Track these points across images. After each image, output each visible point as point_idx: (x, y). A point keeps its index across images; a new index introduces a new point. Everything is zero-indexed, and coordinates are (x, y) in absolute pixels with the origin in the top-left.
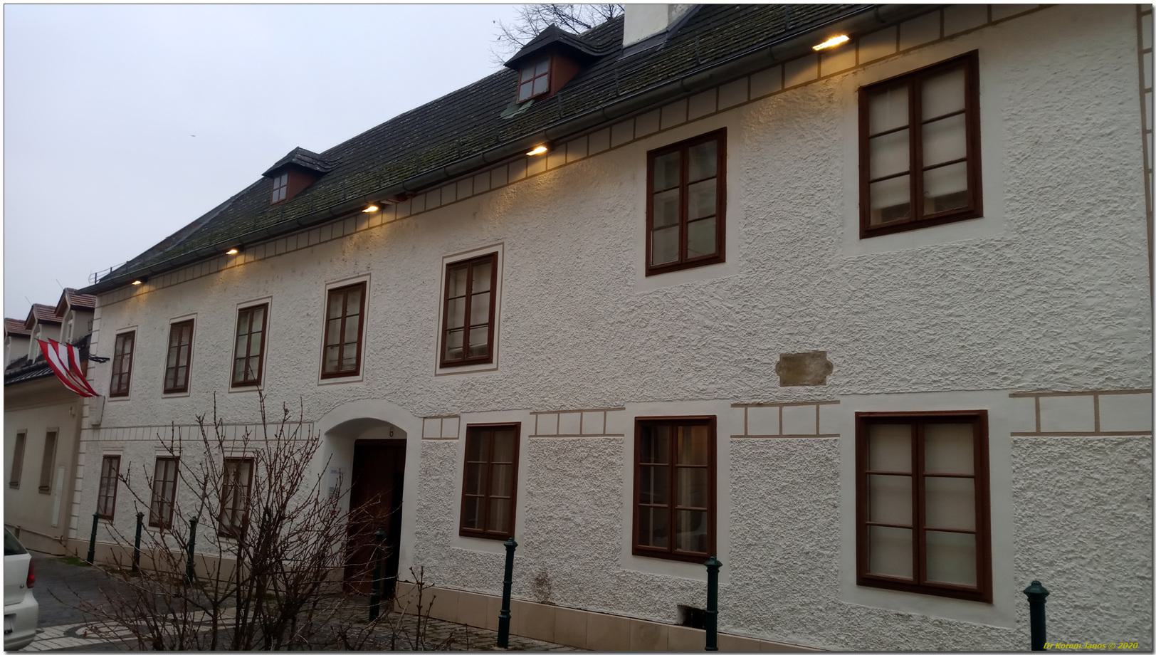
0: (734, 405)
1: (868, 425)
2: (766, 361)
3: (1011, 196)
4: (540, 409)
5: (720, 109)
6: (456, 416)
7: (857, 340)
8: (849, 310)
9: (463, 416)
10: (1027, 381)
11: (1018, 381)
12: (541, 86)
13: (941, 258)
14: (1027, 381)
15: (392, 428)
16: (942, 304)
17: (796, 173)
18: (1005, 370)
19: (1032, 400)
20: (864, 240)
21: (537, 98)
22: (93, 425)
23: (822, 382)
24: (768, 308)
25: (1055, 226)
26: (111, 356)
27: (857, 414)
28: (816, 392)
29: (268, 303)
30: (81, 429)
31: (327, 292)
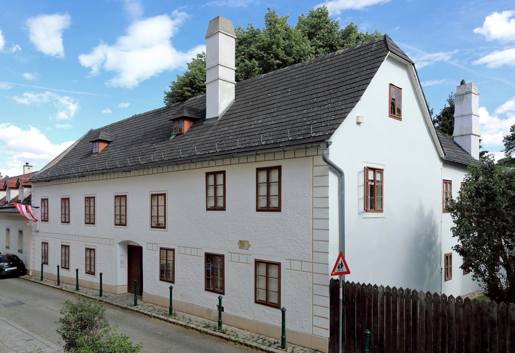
1: (257, 262)
6: (156, 244)
23: (248, 249)
30: (216, 197)
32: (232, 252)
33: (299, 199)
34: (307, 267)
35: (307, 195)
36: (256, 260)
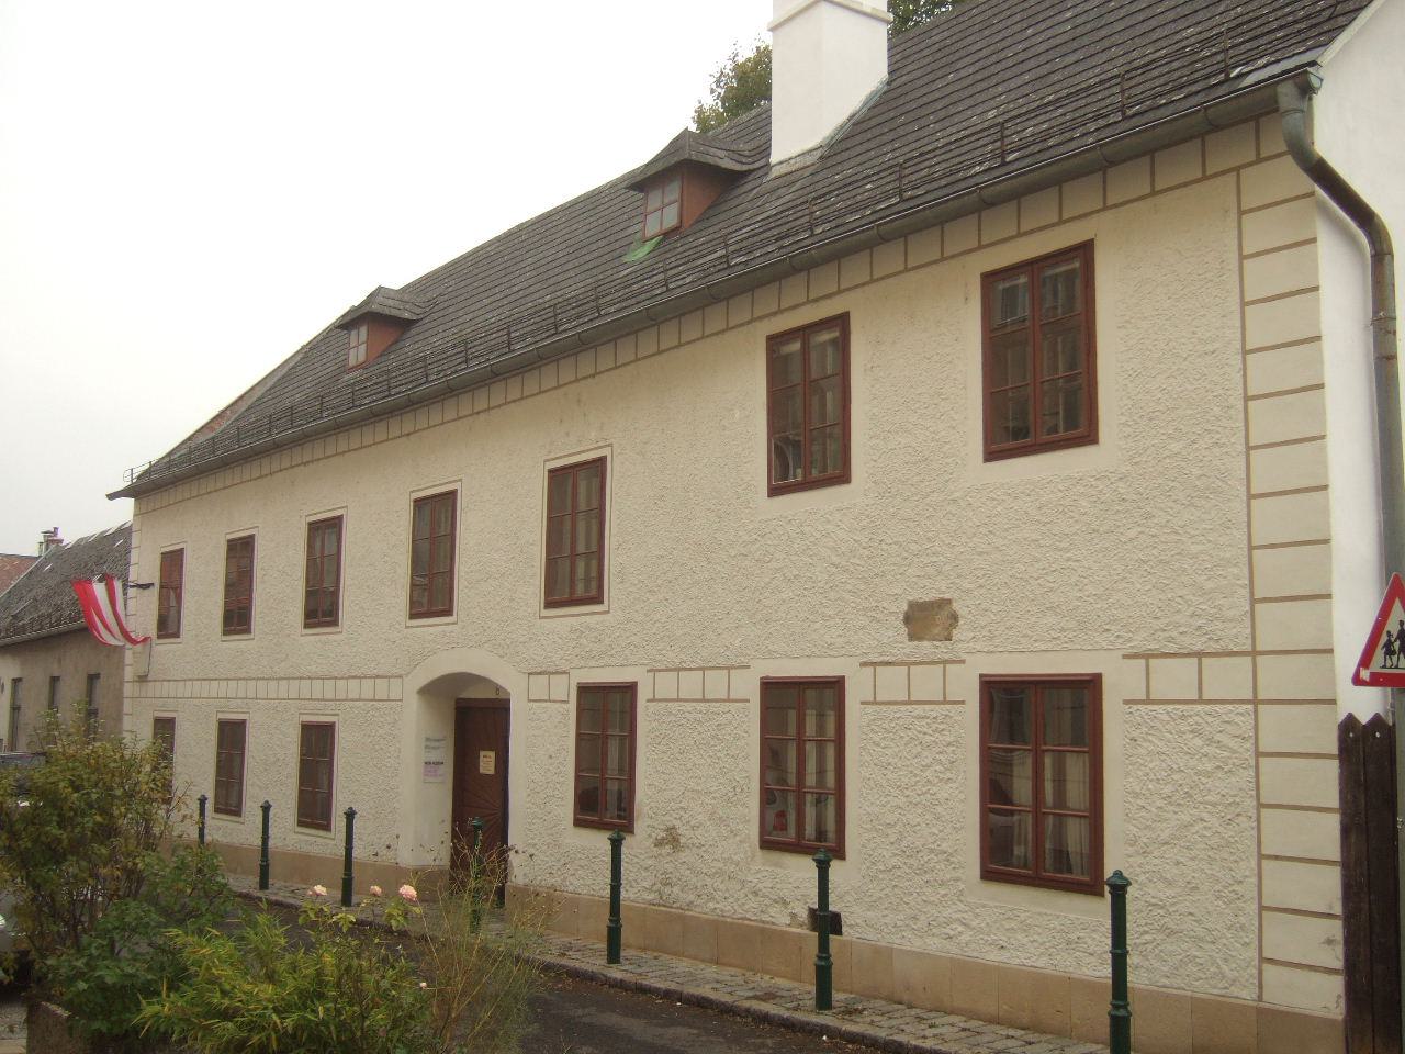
0: (864, 664)
2: (894, 609)
3: (1123, 419)
4: (658, 666)
5: (1065, 216)
6: (564, 672)
7: (981, 586)
8: (974, 549)
9: (571, 671)
10: (1137, 640)
11: (1130, 640)
12: (671, 218)
13: (1060, 490)
14: (1137, 640)
15: (498, 688)
16: (1062, 545)
17: (920, 375)
18: (1119, 627)
19: (1143, 661)
20: (988, 464)
21: (667, 234)
22: (140, 677)
24: (896, 543)
25: (1164, 458)
26: (157, 582)
27: (981, 676)
28: (940, 649)
29: (605, 457)
31: (546, 473)
32: (875, 660)
33: (1178, 369)
34: (1228, 678)
35: (1217, 345)
36: (983, 679)
